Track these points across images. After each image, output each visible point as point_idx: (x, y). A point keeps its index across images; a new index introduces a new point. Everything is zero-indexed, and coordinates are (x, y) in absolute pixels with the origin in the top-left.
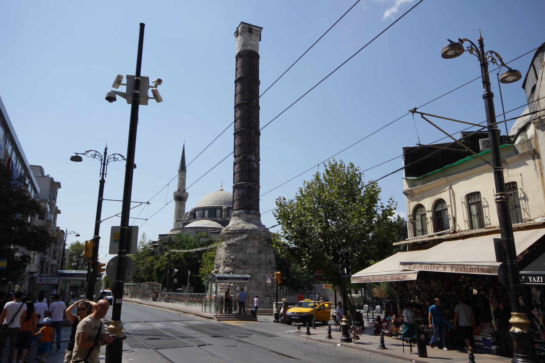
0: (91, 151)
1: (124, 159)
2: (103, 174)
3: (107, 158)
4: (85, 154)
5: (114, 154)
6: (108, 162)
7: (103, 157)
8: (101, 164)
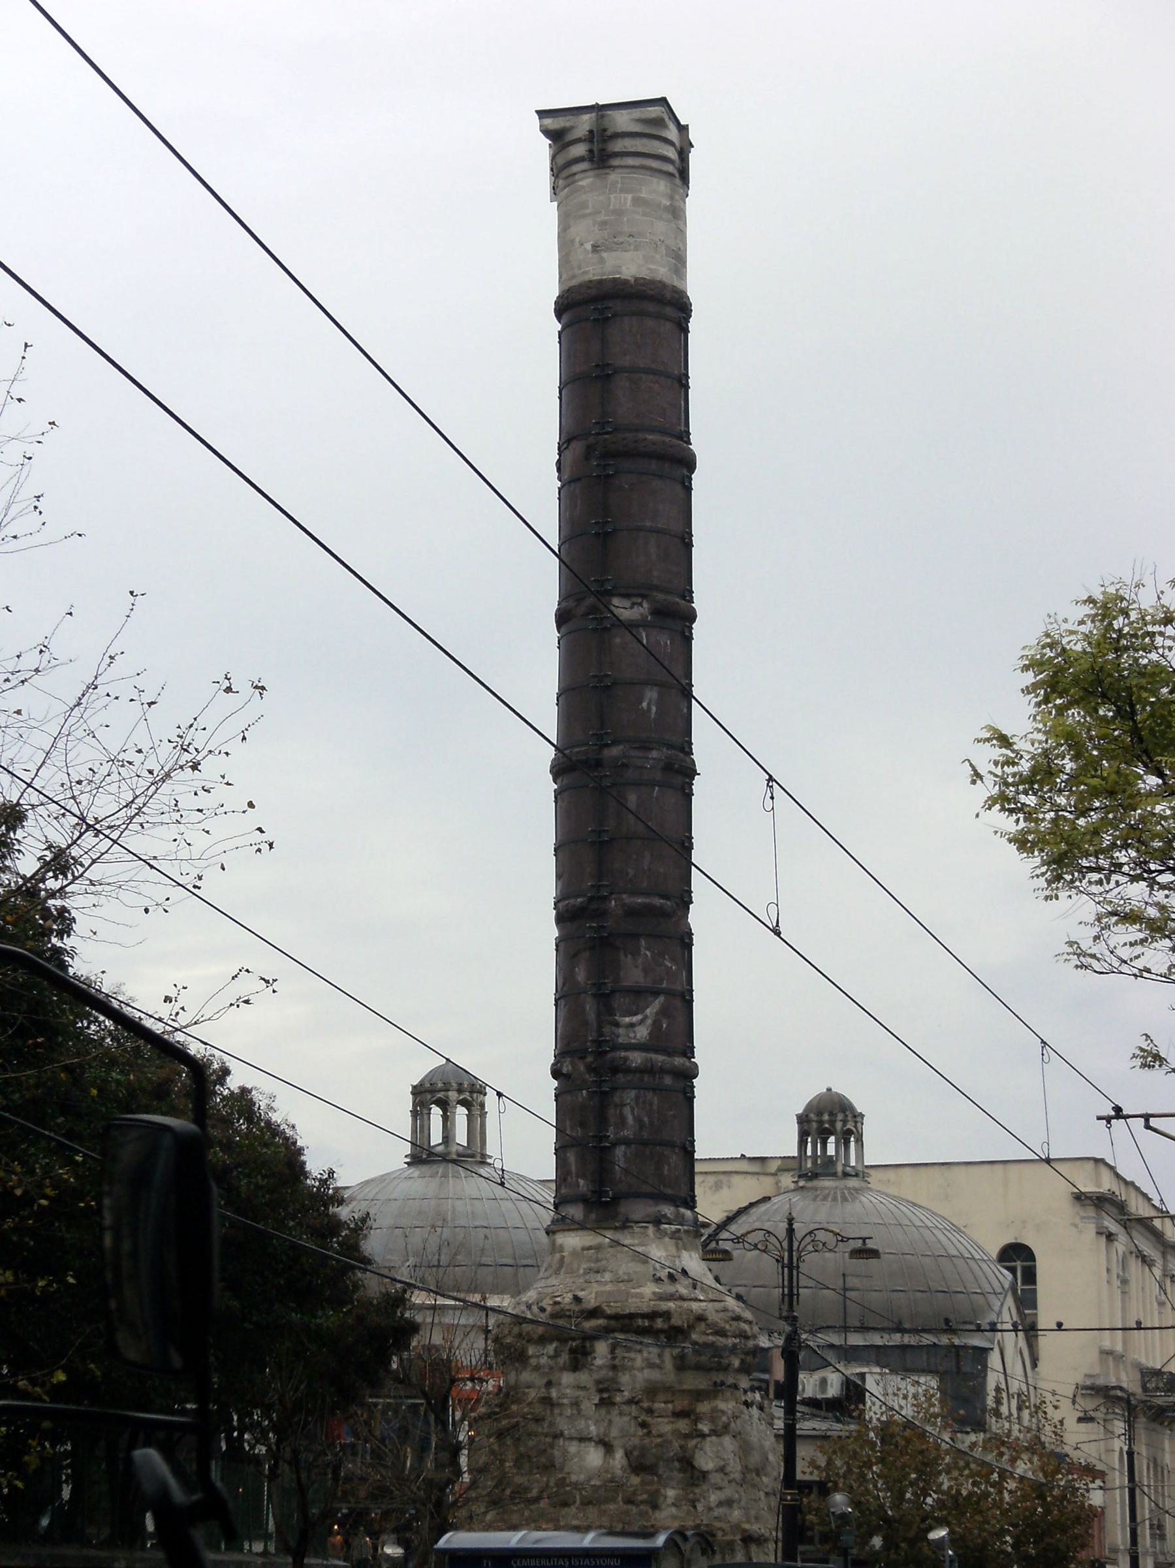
1: (840, 1238)
3: (795, 1248)
5: (811, 1232)
6: (799, 1258)
7: (785, 1244)
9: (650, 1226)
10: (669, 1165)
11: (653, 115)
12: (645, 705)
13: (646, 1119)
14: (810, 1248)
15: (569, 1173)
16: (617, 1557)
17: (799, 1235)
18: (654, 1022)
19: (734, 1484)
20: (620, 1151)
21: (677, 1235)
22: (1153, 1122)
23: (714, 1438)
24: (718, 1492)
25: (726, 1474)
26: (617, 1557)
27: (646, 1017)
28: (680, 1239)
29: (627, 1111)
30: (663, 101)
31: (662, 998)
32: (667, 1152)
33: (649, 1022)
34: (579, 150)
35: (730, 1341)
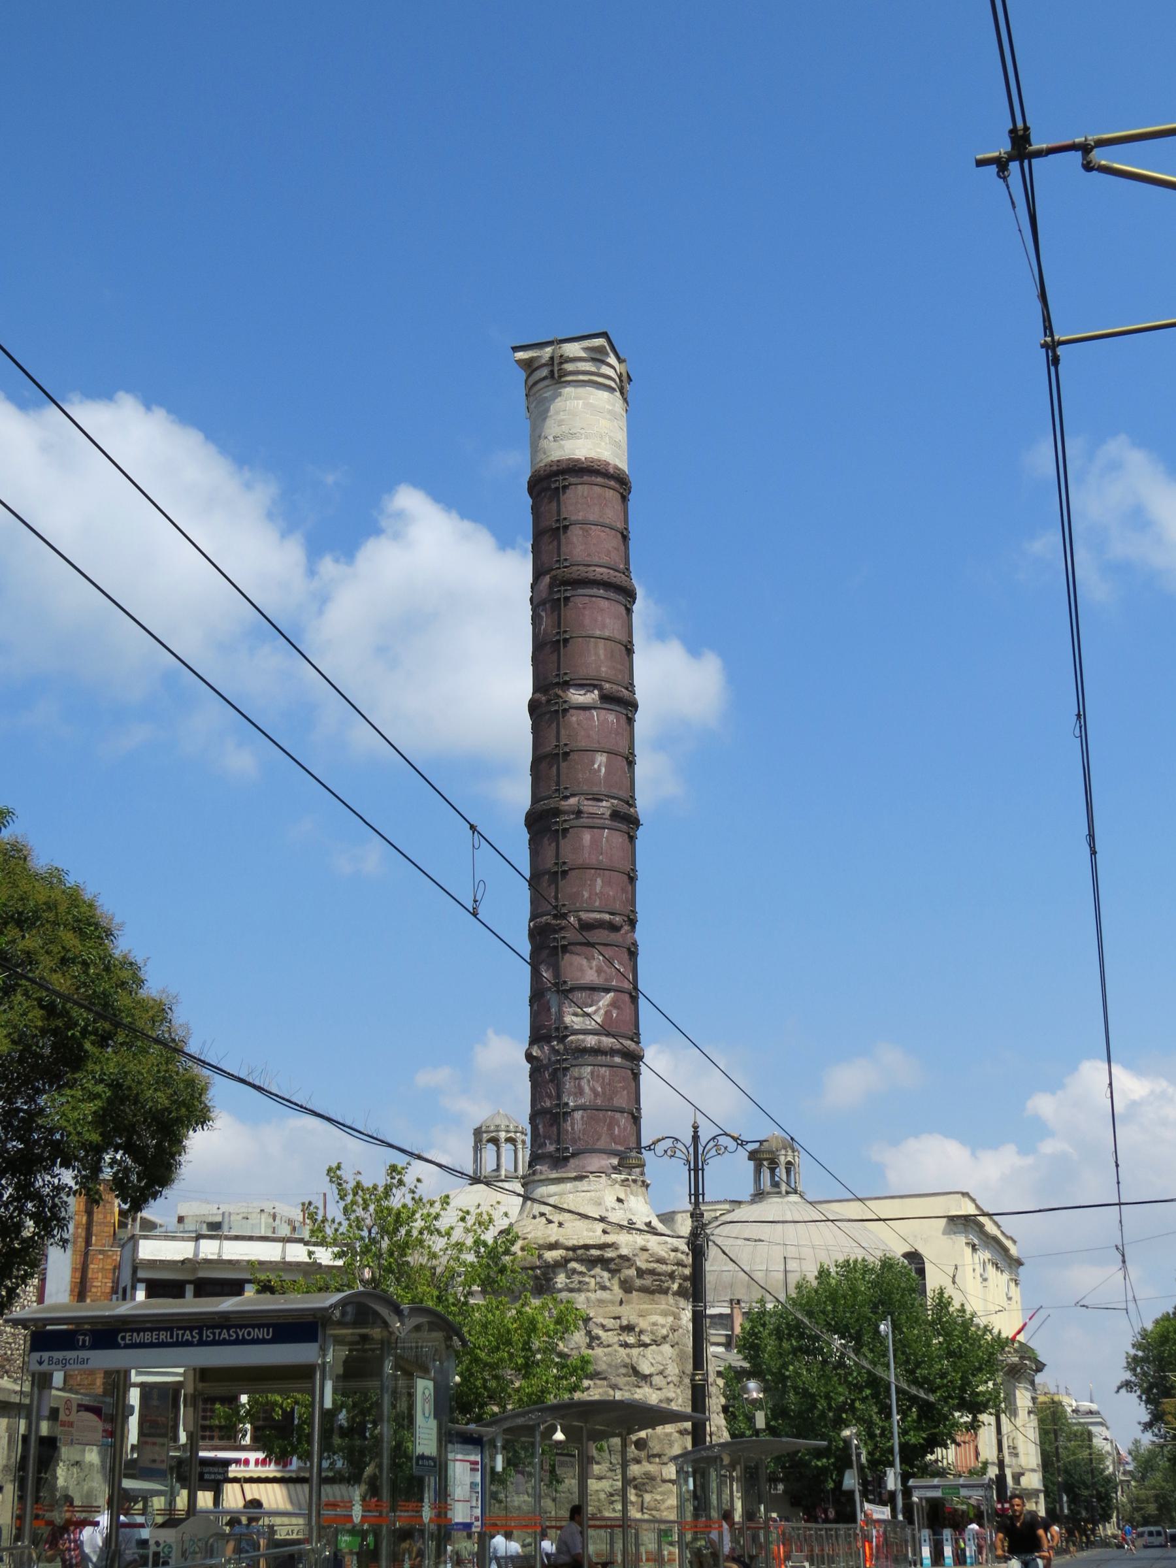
0: (659, 1140)
2: (697, 1195)
3: (700, 1151)
4: (650, 1150)
5: (714, 1138)
7: (691, 1150)
8: (690, 1170)
9: (603, 1175)
10: (619, 1126)
11: (597, 344)
12: (596, 766)
13: (599, 1089)
14: (713, 1152)
15: (539, 1135)
16: (268, 1326)
17: (703, 1140)
18: (606, 1012)
19: (672, 1385)
20: (578, 1115)
21: (626, 1183)
22: (1100, 157)
23: (654, 1347)
24: (658, 1392)
25: (665, 1377)
26: (268, 1326)
27: (599, 1009)
28: (629, 1186)
29: (584, 1083)
30: (604, 335)
31: (612, 994)
32: (618, 1115)
33: (602, 1012)
34: (544, 372)
35: (669, 1268)
